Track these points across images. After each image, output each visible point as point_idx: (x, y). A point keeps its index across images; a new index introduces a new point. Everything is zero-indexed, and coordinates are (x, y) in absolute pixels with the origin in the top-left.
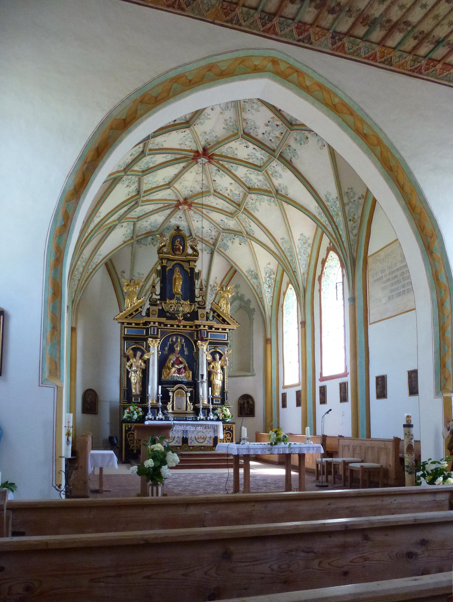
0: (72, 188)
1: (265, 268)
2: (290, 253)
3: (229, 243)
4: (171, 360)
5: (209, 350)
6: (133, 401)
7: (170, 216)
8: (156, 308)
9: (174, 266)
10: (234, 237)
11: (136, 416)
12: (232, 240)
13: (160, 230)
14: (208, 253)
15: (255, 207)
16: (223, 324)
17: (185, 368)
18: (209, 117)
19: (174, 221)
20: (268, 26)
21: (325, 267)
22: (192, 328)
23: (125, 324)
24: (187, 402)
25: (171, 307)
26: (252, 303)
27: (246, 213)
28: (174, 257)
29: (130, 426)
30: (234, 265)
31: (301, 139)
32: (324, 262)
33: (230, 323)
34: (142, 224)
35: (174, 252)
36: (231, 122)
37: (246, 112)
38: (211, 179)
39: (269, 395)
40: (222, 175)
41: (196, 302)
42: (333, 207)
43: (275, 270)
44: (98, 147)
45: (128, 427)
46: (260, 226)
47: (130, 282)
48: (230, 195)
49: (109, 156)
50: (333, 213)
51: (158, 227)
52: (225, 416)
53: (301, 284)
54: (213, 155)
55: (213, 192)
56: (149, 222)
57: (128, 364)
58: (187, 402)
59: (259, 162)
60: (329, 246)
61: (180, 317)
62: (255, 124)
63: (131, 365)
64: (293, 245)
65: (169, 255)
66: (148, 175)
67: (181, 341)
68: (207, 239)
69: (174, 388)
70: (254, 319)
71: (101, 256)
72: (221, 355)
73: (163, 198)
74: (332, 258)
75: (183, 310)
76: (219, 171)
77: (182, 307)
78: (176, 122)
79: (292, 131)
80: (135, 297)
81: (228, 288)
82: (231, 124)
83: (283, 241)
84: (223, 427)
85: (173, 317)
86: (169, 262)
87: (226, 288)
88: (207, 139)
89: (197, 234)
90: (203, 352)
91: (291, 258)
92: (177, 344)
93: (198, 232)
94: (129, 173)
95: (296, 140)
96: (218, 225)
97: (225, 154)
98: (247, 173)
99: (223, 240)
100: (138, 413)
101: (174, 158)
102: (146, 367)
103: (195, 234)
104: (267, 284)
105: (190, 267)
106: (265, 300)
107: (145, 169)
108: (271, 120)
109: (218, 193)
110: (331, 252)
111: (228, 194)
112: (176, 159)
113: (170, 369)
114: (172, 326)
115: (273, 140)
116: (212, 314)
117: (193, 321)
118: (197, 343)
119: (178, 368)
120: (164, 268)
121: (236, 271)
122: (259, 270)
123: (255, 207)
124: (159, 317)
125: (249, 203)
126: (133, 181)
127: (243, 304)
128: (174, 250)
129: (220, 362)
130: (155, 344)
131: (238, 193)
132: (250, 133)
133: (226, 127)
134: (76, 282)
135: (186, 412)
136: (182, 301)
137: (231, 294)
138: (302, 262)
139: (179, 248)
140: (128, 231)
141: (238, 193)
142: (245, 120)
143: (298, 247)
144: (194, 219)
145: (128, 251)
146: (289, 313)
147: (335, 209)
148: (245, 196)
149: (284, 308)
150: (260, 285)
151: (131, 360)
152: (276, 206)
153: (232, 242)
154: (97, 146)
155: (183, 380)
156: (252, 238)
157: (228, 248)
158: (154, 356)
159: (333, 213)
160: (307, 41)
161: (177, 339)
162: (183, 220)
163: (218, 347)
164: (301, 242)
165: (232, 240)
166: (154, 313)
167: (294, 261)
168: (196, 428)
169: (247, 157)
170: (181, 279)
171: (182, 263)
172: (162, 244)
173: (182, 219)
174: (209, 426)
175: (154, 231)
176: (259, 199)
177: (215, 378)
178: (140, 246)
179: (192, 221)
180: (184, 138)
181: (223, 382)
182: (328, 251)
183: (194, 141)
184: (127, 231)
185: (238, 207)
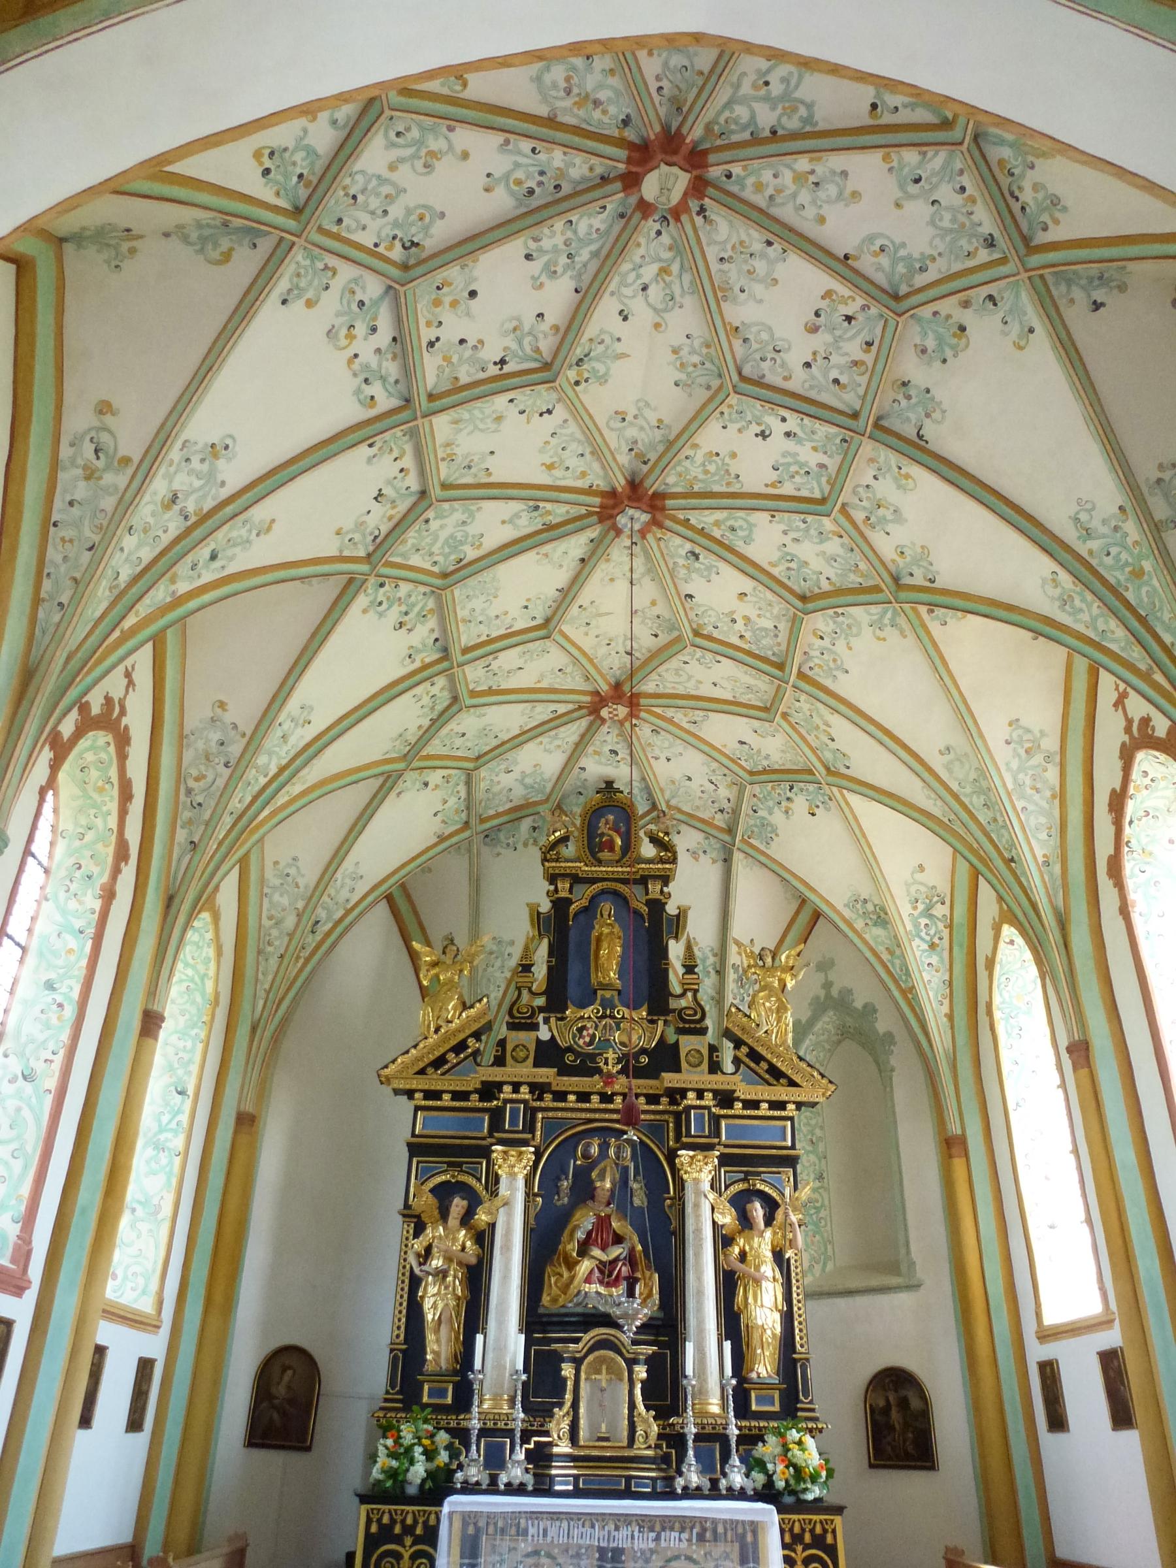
1: (908, 885)
2: (982, 797)
3: (778, 818)
4: (576, 1227)
5: (727, 1187)
6: (425, 1399)
8: (526, 1038)
9: (593, 899)
10: (789, 794)
11: (418, 1471)
12: (784, 803)
13: (554, 797)
14: (714, 861)
15: (835, 660)
16: (770, 1084)
17: (631, 1260)
18: (619, 348)
21: (1127, 820)
22: (658, 1103)
23: (417, 1095)
24: (632, 1406)
25: (580, 1030)
27: (807, 687)
28: (593, 869)
29: (386, 1520)
30: (809, 894)
31: (939, 344)
32: (1118, 802)
34: (496, 779)
36: (693, 352)
37: (735, 299)
38: (679, 595)
39: (985, 1370)
40: (709, 568)
41: (674, 1011)
42: (1114, 551)
43: (944, 888)
45: (379, 1521)
46: (863, 723)
48: (748, 635)
50: (1118, 574)
51: (548, 790)
52: (798, 1470)
53: (1045, 900)
55: (691, 635)
57: (418, 1245)
58: (632, 1406)
59: (815, 485)
60: (1126, 738)
62: (772, 335)
63: (428, 1250)
65: (578, 864)
69: (581, 1345)
70: (892, 1070)
71: (360, 882)
72: (771, 1206)
73: (544, 685)
74: (1147, 781)
75: (625, 1039)
76: (697, 557)
77: (618, 1028)
78: (507, 369)
79: (900, 315)
80: (452, 999)
81: (783, 958)
82: (696, 359)
83: (947, 758)
85: (587, 1066)
86: (579, 889)
87: (773, 959)
88: (636, 442)
89: (673, 802)
90: (699, 1193)
91: (990, 814)
92: (602, 1165)
95: (924, 351)
96: (733, 761)
97: (701, 485)
98: (787, 540)
99: (755, 811)
100: (430, 1455)
101: (540, 527)
103: (667, 802)
104: (922, 939)
105: (650, 897)
106: (923, 992)
108: (823, 304)
109: (710, 638)
110: (1140, 756)
111: (741, 637)
113: (571, 1265)
114: (584, 1097)
115: (843, 379)
116: (728, 1046)
117: (656, 1077)
118: (677, 1161)
119: (604, 1257)
120: (561, 905)
121: (817, 915)
122: (888, 897)
123: (835, 660)
125: (812, 653)
126: (416, 609)
127: (849, 1021)
128: (594, 845)
129: (768, 1234)
130: (514, 1166)
131: (769, 625)
132: (763, 376)
133: (683, 377)
134: (273, 962)
135: (627, 1453)
136: (621, 1011)
137: (794, 976)
140: (449, 804)
141: (769, 625)
142: (737, 328)
143: (1009, 769)
144: (657, 752)
145: (458, 867)
146: (1016, 1031)
147: (1124, 556)
148: (795, 624)
149: (997, 1015)
150: (899, 946)
151: (429, 1231)
152: (905, 637)
153: (786, 812)
156: (844, 783)
157: (777, 835)
158: (510, 1215)
159: (1118, 574)
161: (604, 1147)
162: (623, 759)
163: (759, 1174)
164: (1015, 749)
165: (784, 803)
166: (522, 1054)
167: (1000, 820)
168: (657, 1539)
169: (773, 476)
172: (557, 834)
174: (720, 1529)
175: (536, 804)
176: (842, 630)
177: (751, 1300)
179: (652, 761)
181: (788, 1318)
182: (1127, 757)
183: (592, 453)
184: (445, 802)
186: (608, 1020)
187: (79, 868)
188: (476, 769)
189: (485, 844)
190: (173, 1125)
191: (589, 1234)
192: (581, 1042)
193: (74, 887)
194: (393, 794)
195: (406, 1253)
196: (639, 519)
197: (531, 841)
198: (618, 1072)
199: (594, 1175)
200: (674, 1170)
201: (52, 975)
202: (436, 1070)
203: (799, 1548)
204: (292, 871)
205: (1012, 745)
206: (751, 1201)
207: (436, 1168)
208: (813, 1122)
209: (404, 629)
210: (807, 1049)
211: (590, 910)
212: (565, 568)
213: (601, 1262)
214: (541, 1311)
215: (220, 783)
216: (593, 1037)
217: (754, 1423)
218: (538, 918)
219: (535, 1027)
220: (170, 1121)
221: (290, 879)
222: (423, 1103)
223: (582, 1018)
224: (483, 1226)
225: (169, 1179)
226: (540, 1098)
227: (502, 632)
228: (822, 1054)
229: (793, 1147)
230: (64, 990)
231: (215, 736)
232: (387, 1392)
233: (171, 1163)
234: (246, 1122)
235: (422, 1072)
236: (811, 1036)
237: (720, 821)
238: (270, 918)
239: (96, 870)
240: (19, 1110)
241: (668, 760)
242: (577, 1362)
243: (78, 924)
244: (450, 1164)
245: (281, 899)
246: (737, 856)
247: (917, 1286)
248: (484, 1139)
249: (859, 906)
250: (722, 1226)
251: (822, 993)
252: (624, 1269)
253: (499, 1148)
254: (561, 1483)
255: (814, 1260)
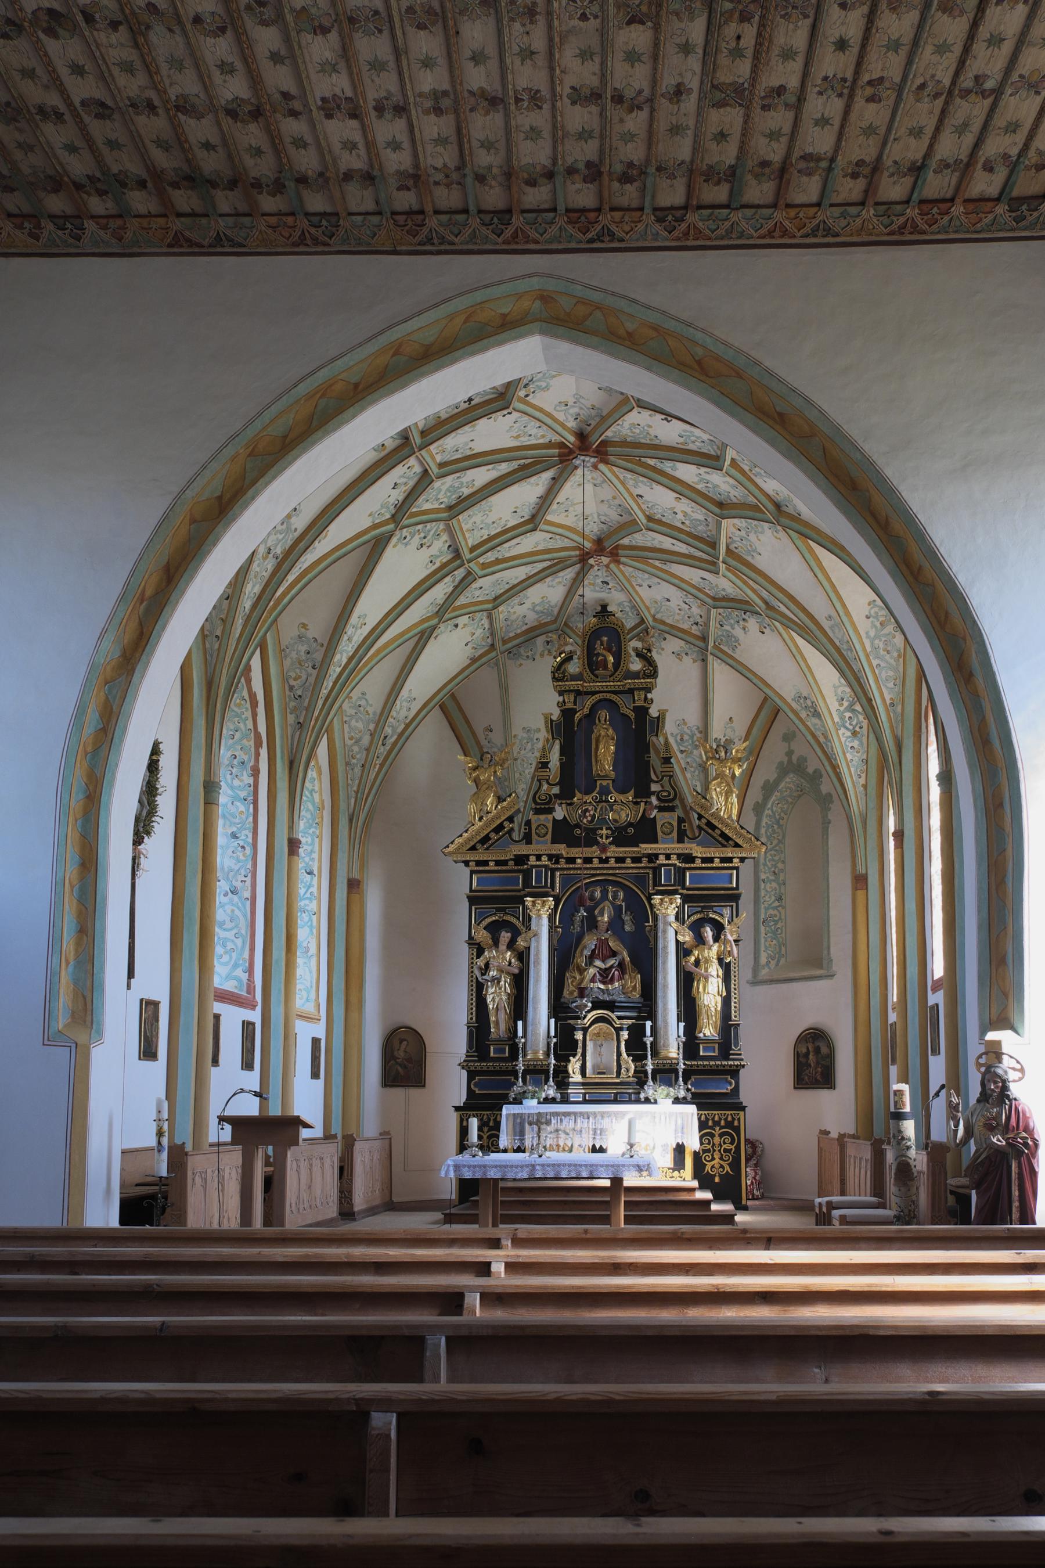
0: (117, 654)
3: (738, 632)
4: (585, 947)
5: (689, 917)
7: (578, 580)
8: (546, 819)
9: (594, 708)
10: (744, 616)
12: (741, 622)
13: (559, 621)
15: (751, 546)
17: (621, 966)
19: (591, 593)
20: (508, 232)
22: (641, 862)
24: (619, 1054)
26: (825, 779)
33: (740, 842)
34: (512, 611)
35: (592, 672)
41: (653, 793)
44: (168, 563)
47: (482, 759)
48: (687, 522)
49: (192, 577)
51: (556, 611)
54: (605, 443)
55: (644, 521)
56: (528, 604)
57: (481, 962)
58: (619, 1054)
61: (604, 837)
63: (487, 965)
64: (851, 632)
66: (470, 512)
67: (615, 897)
68: (685, 626)
71: (414, 703)
72: (719, 929)
73: (540, 548)
75: (617, 817)
77: (612, 810)
78: (473, 403)
84: (699, 1119)
87: (726, 753)
88: (579, 414)
89: (658, 616)
92: (602, 906)
93: (658, 613)
94: (405, 522)
99: (721, 625)
102: (521, 971)
103: (654, 617)
104: (847, 729)
106: (846, 770)
107: (454, 502)
109: (659, 522)
111: (683, 523)
112: (523, 468)
113: (581, 971)
114: (588, 860)
119: (603, 966)
120: (567, 714)
124: (554, 842)
126: (432, 533)
128: (593, 663)
130: (539, 910)
137: (740, 766)
138: (884, 675)
139: (605, 661)
143: (868, 637)
154: (166, 561)
155: (615, 997)
157: (739, 644)
158: (538, 942)
160: (608, 238)
161: (605, 892)
163: (711, 907)
164: (872, 622)
165: (741, 622)
166: (543, 831)
170: (613, 739)
171: (613, 697)
173: (610, 587)
176: (752, 528)
178: (518, 663)
179: (637, 588)
180: (517, 425)
181: (726, 1001)
185: (710, 550)
186: (604, 804)
187: (235, 758)
188: (495, 608)
189: (509, 658)
190: (308, 895)
191: (593, 951)
192: (585, 821)
193: (234, 770)
194: (432, 639)
195: (472, 968)
196: (588, 461)
197: (546, 652)
198: (610, 843)
199: (596, 912)
200: (652, 906)
201: (235, 829)
202: (483, 845)
203: (717, 1128)
204: (363, 703)
205: (871, 619)
206: (704, 927)
207: (488, 912)
208: (776, 858)
209: (424, 547)
210: (773, 803)
211: (591, 717)
212: (541, 485)
213: (600, 969)
214: (562, 1000)
215: (312, 680)
216: (593, 817)
217: (700, 1063)
218: (551, 724)
219: (550, 811)
220: (306, 893)
221: (361, 709)
222: (476, 868)
223: (586, 802)
224: (522, 949)
225: (311, 931)
226: (557, 862)
227: (499, 530)
228: (785, 806)
229: (737, 888)
230: (243, 837)
231: (303, 648)
232: (468, 1052)
233: (311, 920)
234: (354, 885)
235: (473, 848)
236: (776, 793)
237: (695, 630)
238: (351, 738)
239: (246, 758)
240: (233, 911)
241: (650, 587)
242: (585, 1030)
243: (243, 794)
244: (498, 909)
245: (357, 724)
246: (710, 658)
247: (832, 976)
248: (519, 891)
249: (802, 701)
250: (684, 943)
251: (786, 759)
252: (616, 973)
253: (528, 899)
254: (573, 1097)
255: (771, 957)
